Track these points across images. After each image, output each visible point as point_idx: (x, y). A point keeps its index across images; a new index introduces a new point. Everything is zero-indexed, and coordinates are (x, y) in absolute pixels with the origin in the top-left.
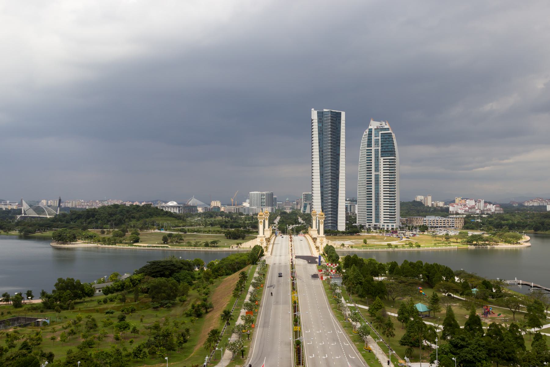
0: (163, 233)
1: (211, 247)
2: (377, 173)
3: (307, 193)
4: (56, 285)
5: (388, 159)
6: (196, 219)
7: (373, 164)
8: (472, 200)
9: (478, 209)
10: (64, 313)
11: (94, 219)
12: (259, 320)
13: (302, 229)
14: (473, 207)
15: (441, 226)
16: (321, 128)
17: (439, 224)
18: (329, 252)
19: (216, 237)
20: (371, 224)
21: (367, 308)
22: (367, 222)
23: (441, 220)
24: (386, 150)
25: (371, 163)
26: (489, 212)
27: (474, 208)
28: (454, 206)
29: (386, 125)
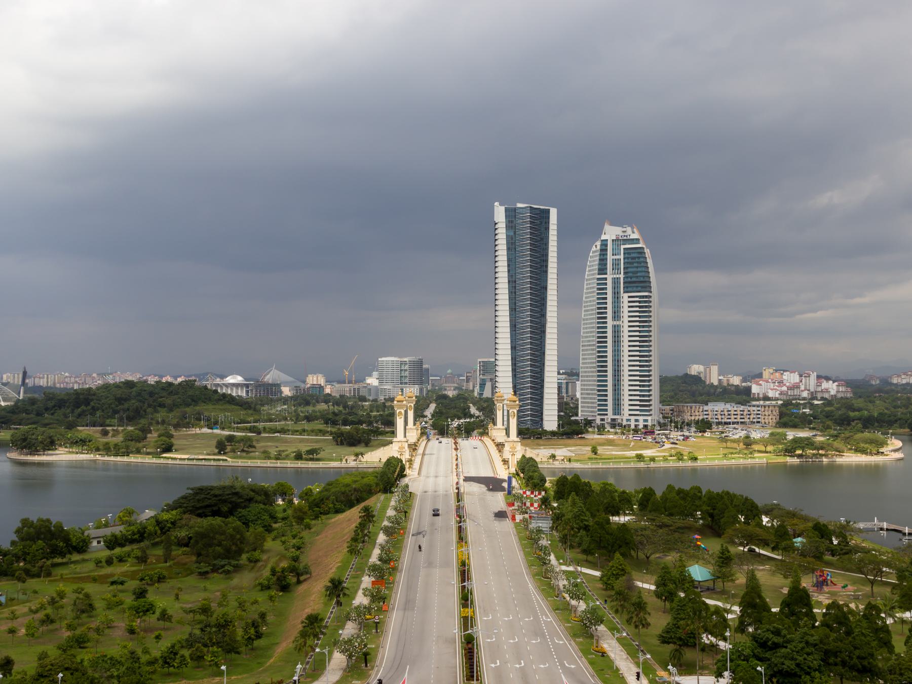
1: (307, 460)
4: (18, 531)
6: (279, 409)
8: (795, 372)
11: (89, 407)
15: (736, 420)
16: (512, 239)
17: (733, 417)
19: (317, 441)
20: (605, 417)
21: (597, 574)
22: (599, 414)
23: (735, 411)
24: (634, 279)
25: (606, 303)
26: (826, 396)
27: (798, 387)
28: (761, 385)
29: (633, 232)
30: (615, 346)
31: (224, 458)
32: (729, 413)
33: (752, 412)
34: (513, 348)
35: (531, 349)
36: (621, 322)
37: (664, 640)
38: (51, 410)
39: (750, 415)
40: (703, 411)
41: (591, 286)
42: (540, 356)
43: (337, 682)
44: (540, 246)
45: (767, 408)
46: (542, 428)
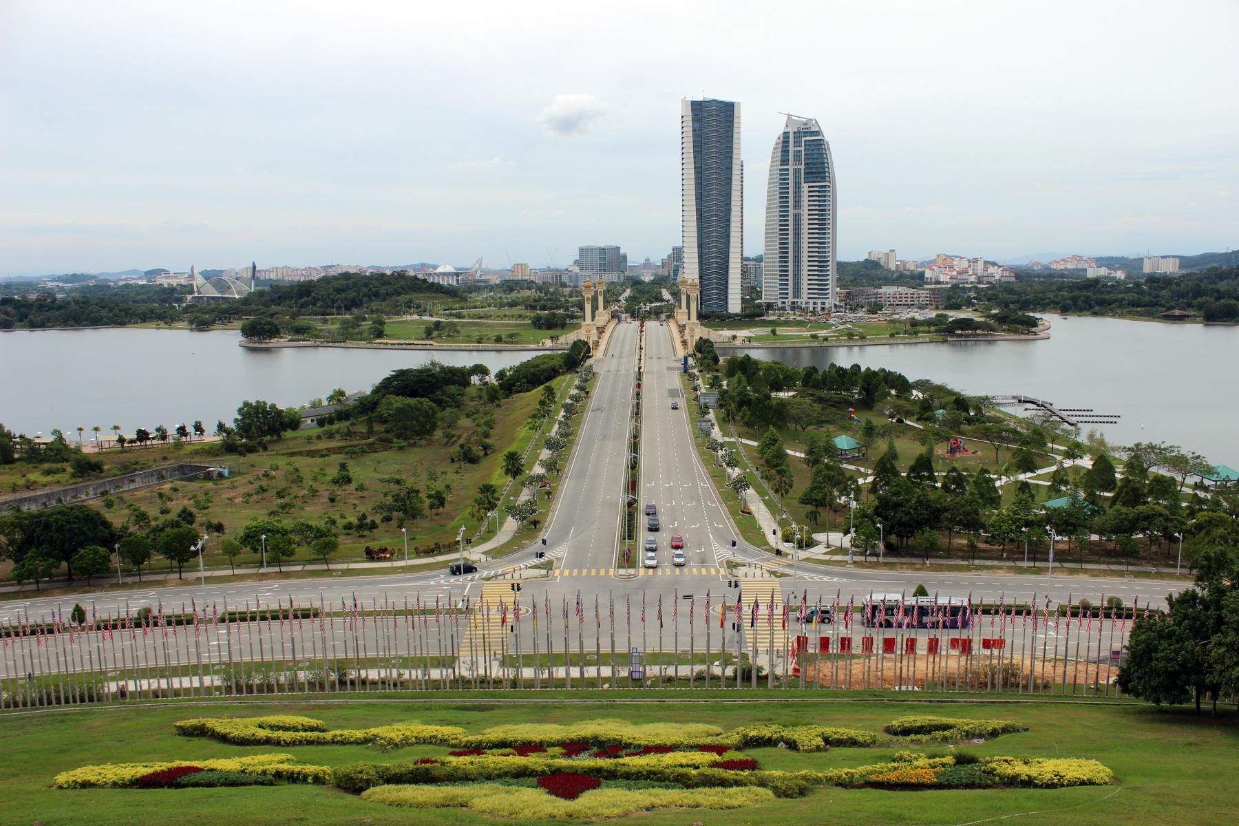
0: (426, 322)
1: (506, 343)
4: (240, 410)
5: (816, 187)
6: (485, 296)
7: (791, 195)
10: (252, 458)
11: (310, 299)
12: (570, 467)
13: (664, 313)
14: (965, 271)
18: (704, 347)
19: (517, 326)
20: (786, 300)
21: (755, 444)
24: (814, 170)
26: (992, 280)
28: (933, 270)
31: (431, 342)
37: (805, 501)
38: (339, 298)
43: (509, 541)
46: (727, 311)
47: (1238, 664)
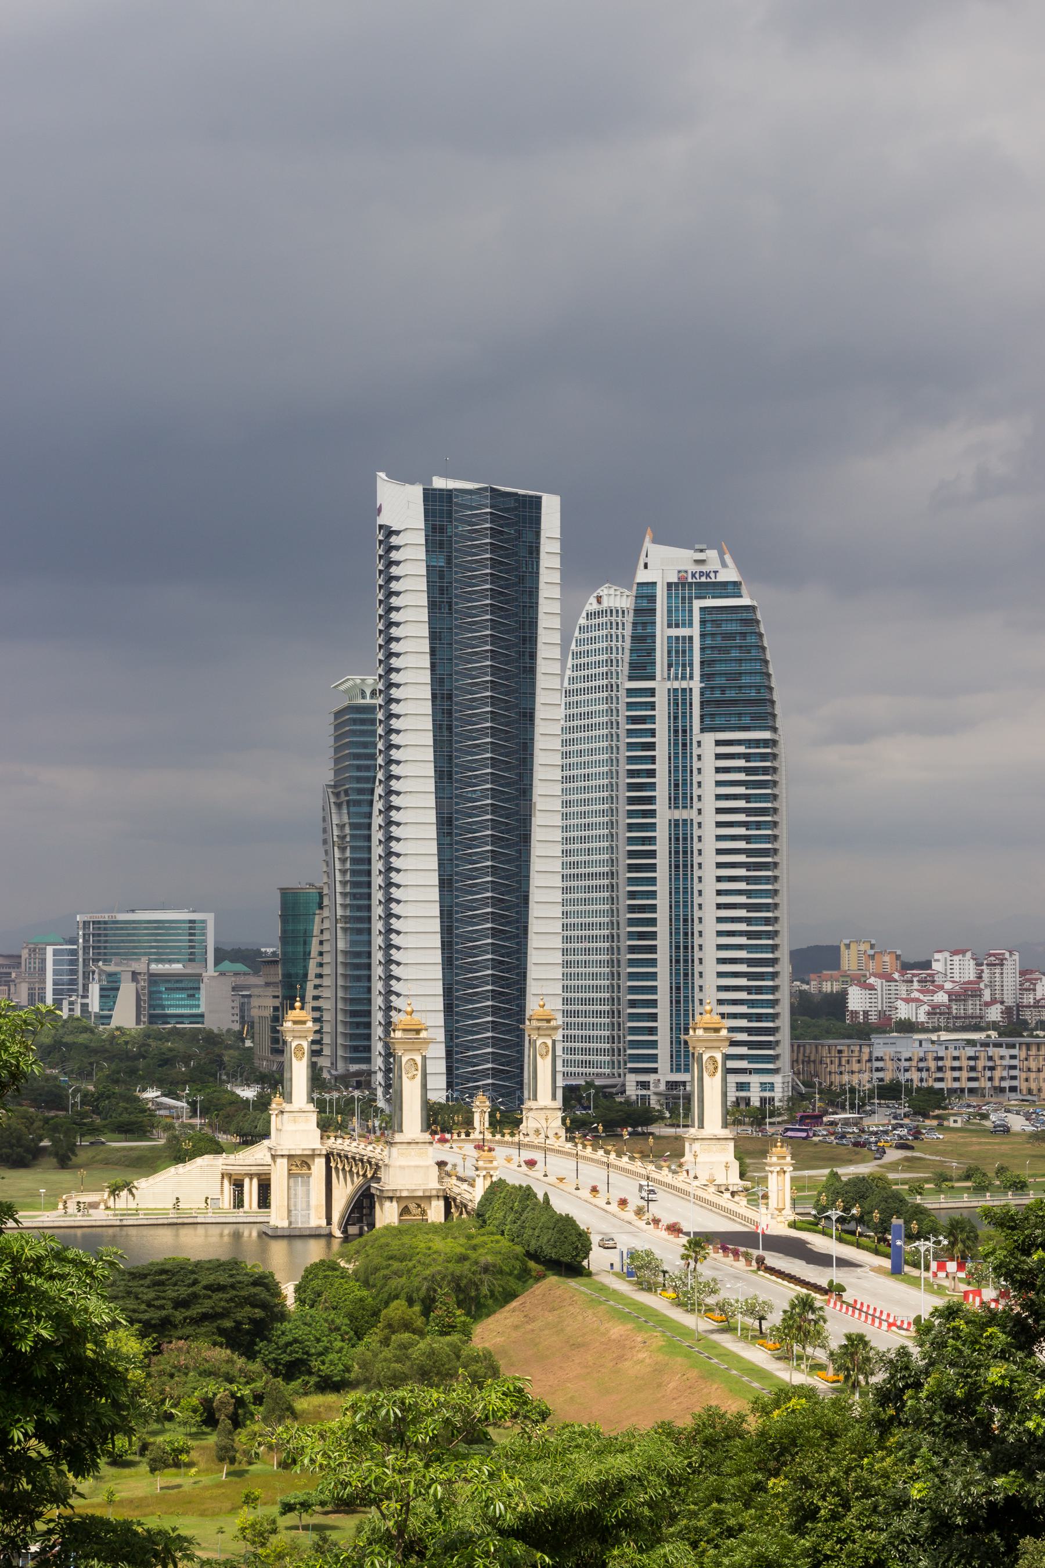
2: (680, 814)
3: (106, 917)
8: (963, 952)
9: (993, 1001)
15: (956, 1085)
16: (442, 577)
17: (949, 1075)
20: (651, 1078)
22: (634, 1071)
23: (955, 1058)
24: (731, 694)
25: (652, 760)
27: (977, 994)
28: (872, 988)
29: (724, 565)
30: (677, 879)
32: (940, 1063)
33: (998, 1062)
34: (446, 884)
35: (495, 886)
36: (695, 811)
39: (992, 1069)
40: (870, 1060)
41: (582, 710)
42: (517, 905)
44: (516, 599)
45: (1033, 1051)
47: (659, 1566)
